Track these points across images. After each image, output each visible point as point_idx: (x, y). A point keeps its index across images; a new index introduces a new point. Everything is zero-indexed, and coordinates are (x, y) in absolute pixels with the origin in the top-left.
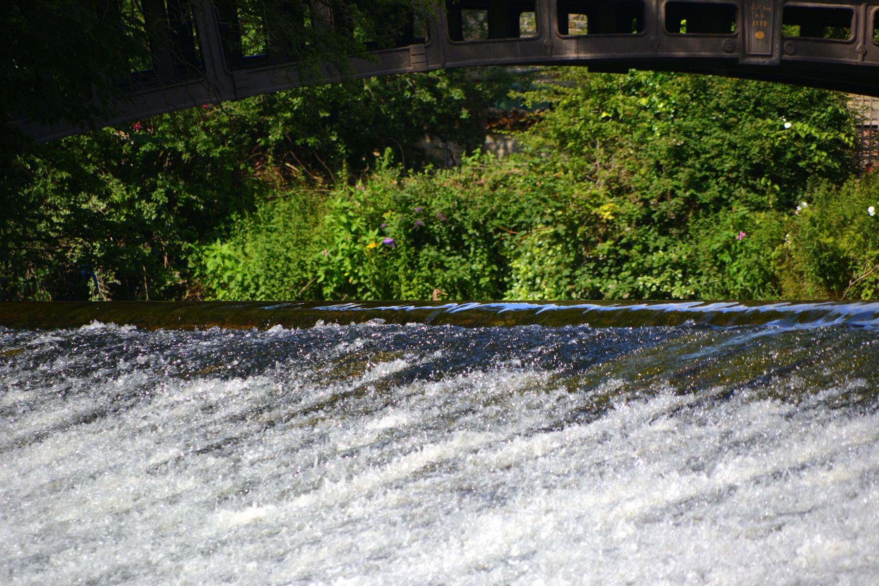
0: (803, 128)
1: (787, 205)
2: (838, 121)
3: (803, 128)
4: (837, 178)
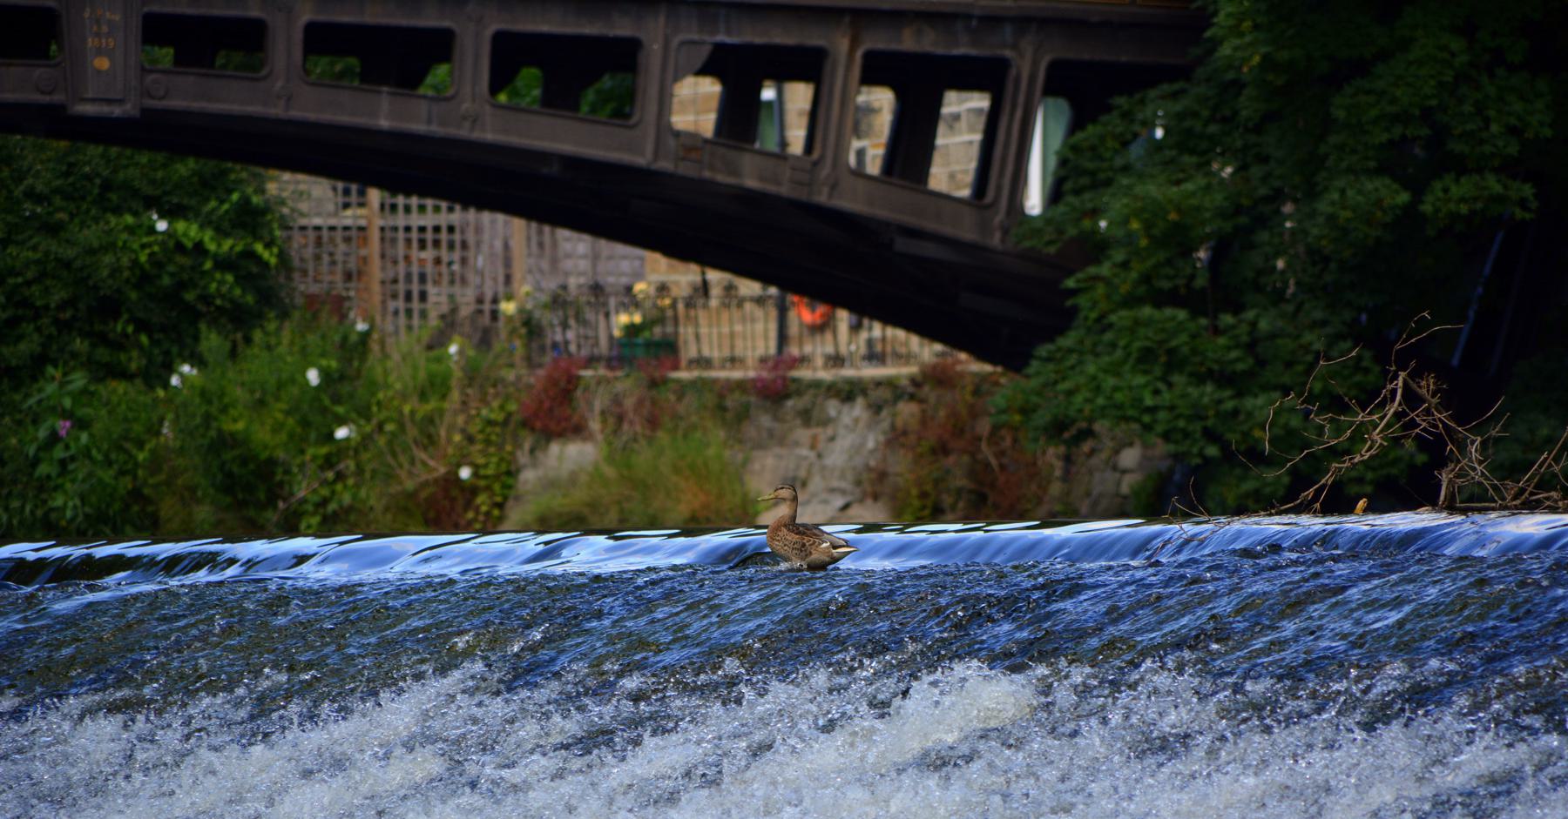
0: (189, 230)
1: (157, 374)
2: (251, 219)
3: (189, 230)
4: (240, 320)
